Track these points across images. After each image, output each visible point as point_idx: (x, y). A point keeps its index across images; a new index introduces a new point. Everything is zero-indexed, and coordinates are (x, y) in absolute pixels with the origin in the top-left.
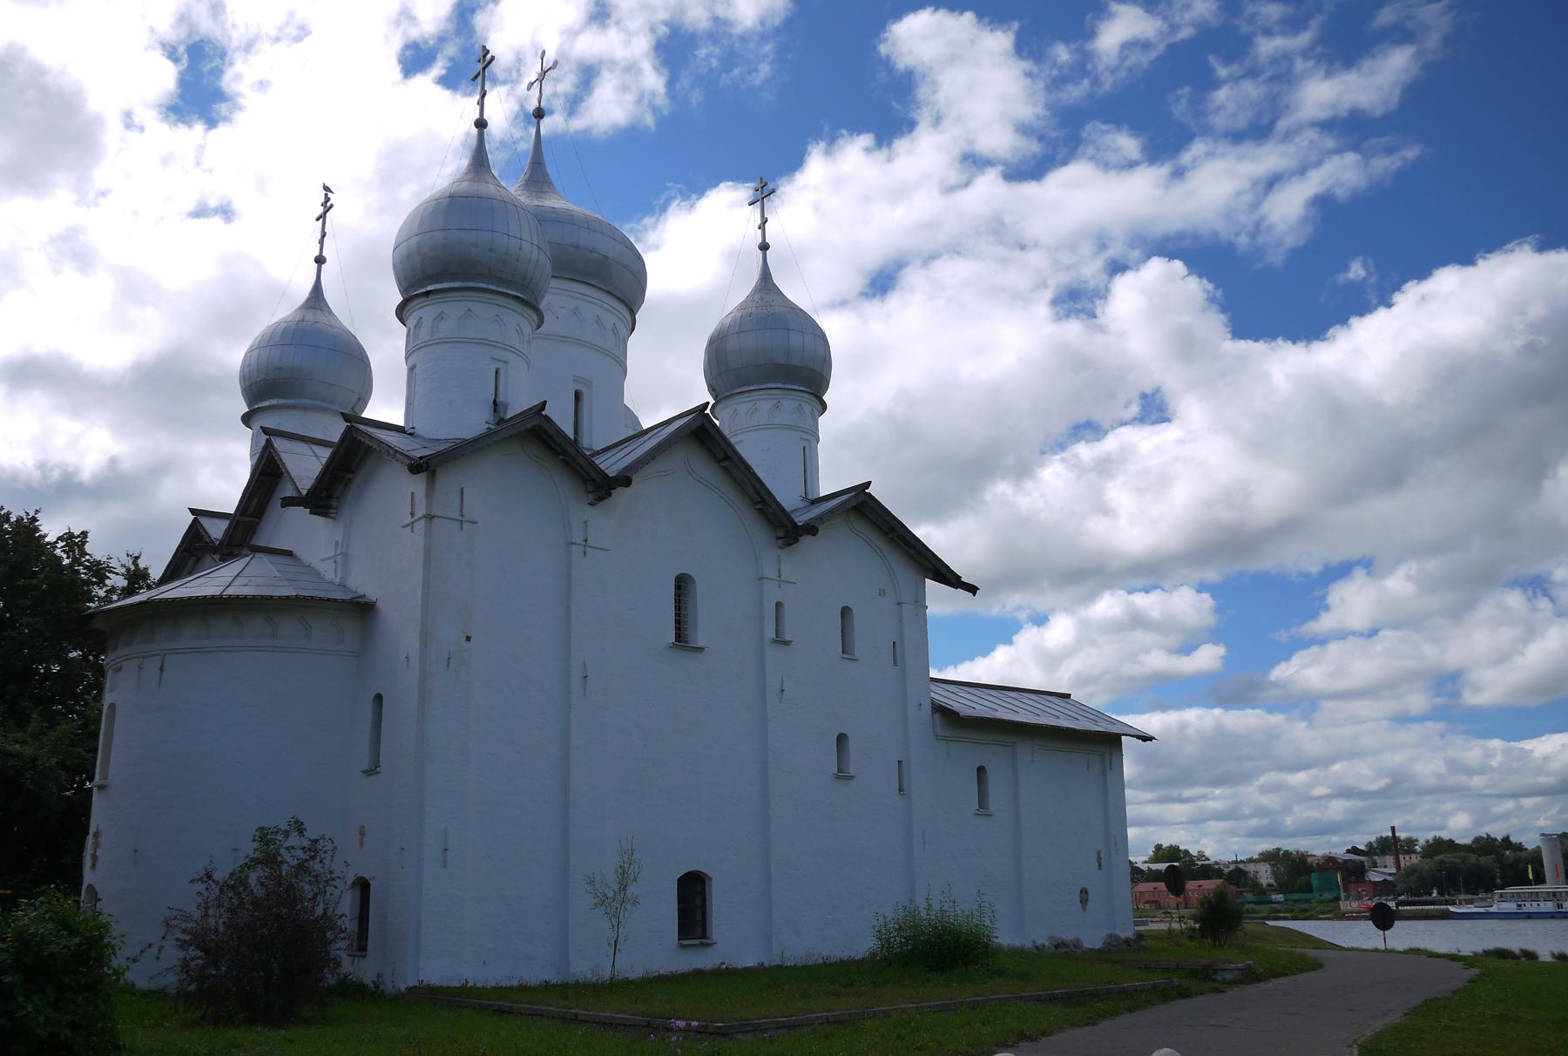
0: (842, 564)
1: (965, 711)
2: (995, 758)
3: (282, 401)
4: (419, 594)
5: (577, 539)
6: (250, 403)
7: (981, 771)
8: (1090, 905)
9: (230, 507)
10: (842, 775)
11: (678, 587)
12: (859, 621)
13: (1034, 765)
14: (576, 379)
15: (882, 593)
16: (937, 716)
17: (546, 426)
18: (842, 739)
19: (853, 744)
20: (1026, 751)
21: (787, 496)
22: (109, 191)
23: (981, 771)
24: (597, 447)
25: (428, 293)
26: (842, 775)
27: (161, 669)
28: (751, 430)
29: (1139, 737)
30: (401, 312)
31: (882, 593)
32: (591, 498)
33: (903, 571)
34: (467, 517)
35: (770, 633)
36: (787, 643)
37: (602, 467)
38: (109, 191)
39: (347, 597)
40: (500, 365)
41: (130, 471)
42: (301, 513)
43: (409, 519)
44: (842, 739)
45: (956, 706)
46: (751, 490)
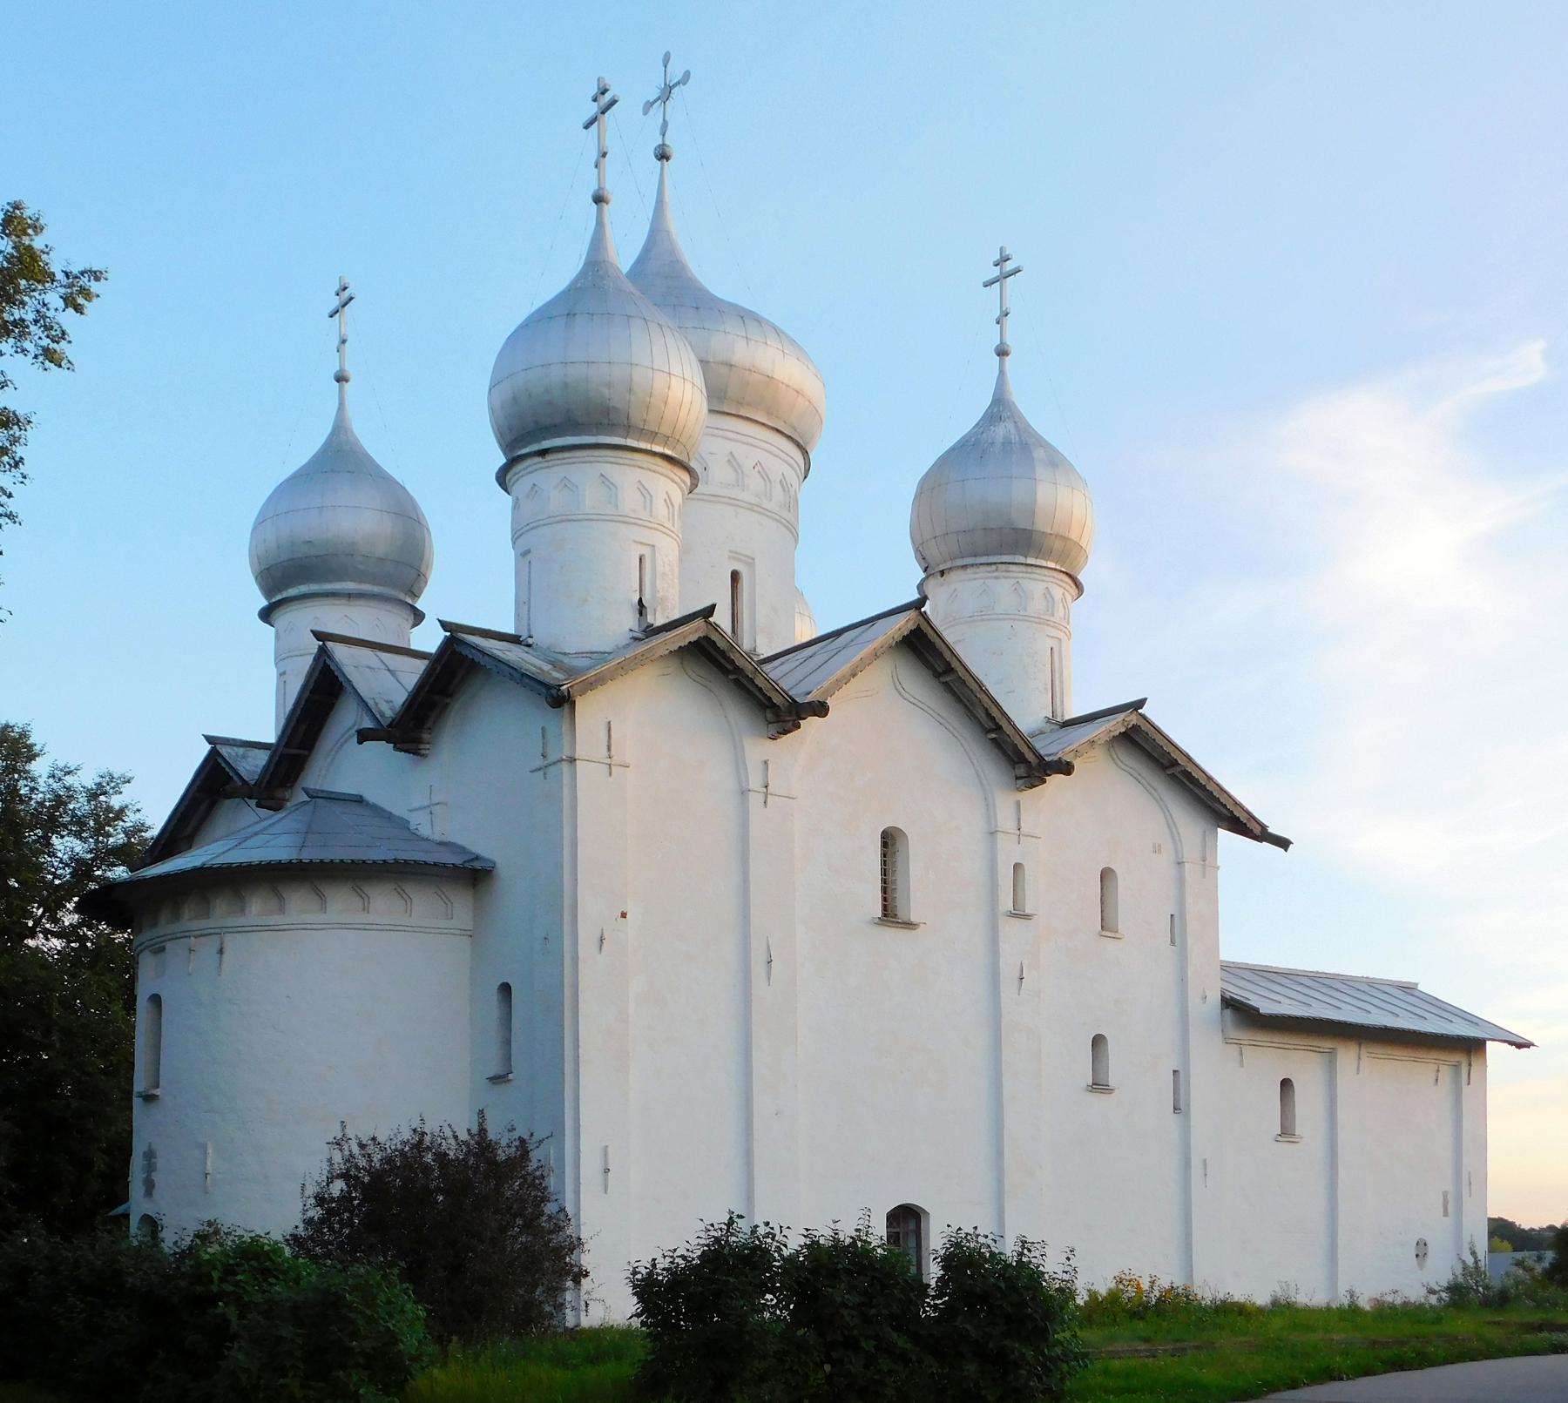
0: (1098, 809)
1: (1266, 1008)
2: (1302, 1063)
3: (314, 587)
4: (1190, 941)
5: (755, 782)
6: (268, 591)
7: (1286, 1084)
8: (1430, 1261)
9: (270, 737)
10: (1099, 1085)
11: (885, 845)
12: (1124, 885)
13: (1365, 1078)
14: (734, 555)
15: (1157, 849)
16: (1228, 1012)
17: (714, 637)
18: (1098, 1041)
19: (1112, 1047)
20: (1347, 1055)
21: (1026, 713)
22: (714, 606)
23: (1286, 1084)
24: (765, 651)
25: (543, 453)
26: (1099, 1085)
27: (221, 952)
28: (968, 618)
29: (1511, 1043)
30: (502, 478)
31: (1157, 849)
32: (773, 729)
33: (1188, 823)
34: (616, 759)
35: (1006, 903)
36: (1027, 917)
37: (785, 684)
38: (714, 606)
39: (458, 861)
40: (646, 551)
41: (139, 696)
42: (380, 750)
43: (539, 762)
44: (1098, 1041)
45: (1254, 1001)
46: (981, 714)
